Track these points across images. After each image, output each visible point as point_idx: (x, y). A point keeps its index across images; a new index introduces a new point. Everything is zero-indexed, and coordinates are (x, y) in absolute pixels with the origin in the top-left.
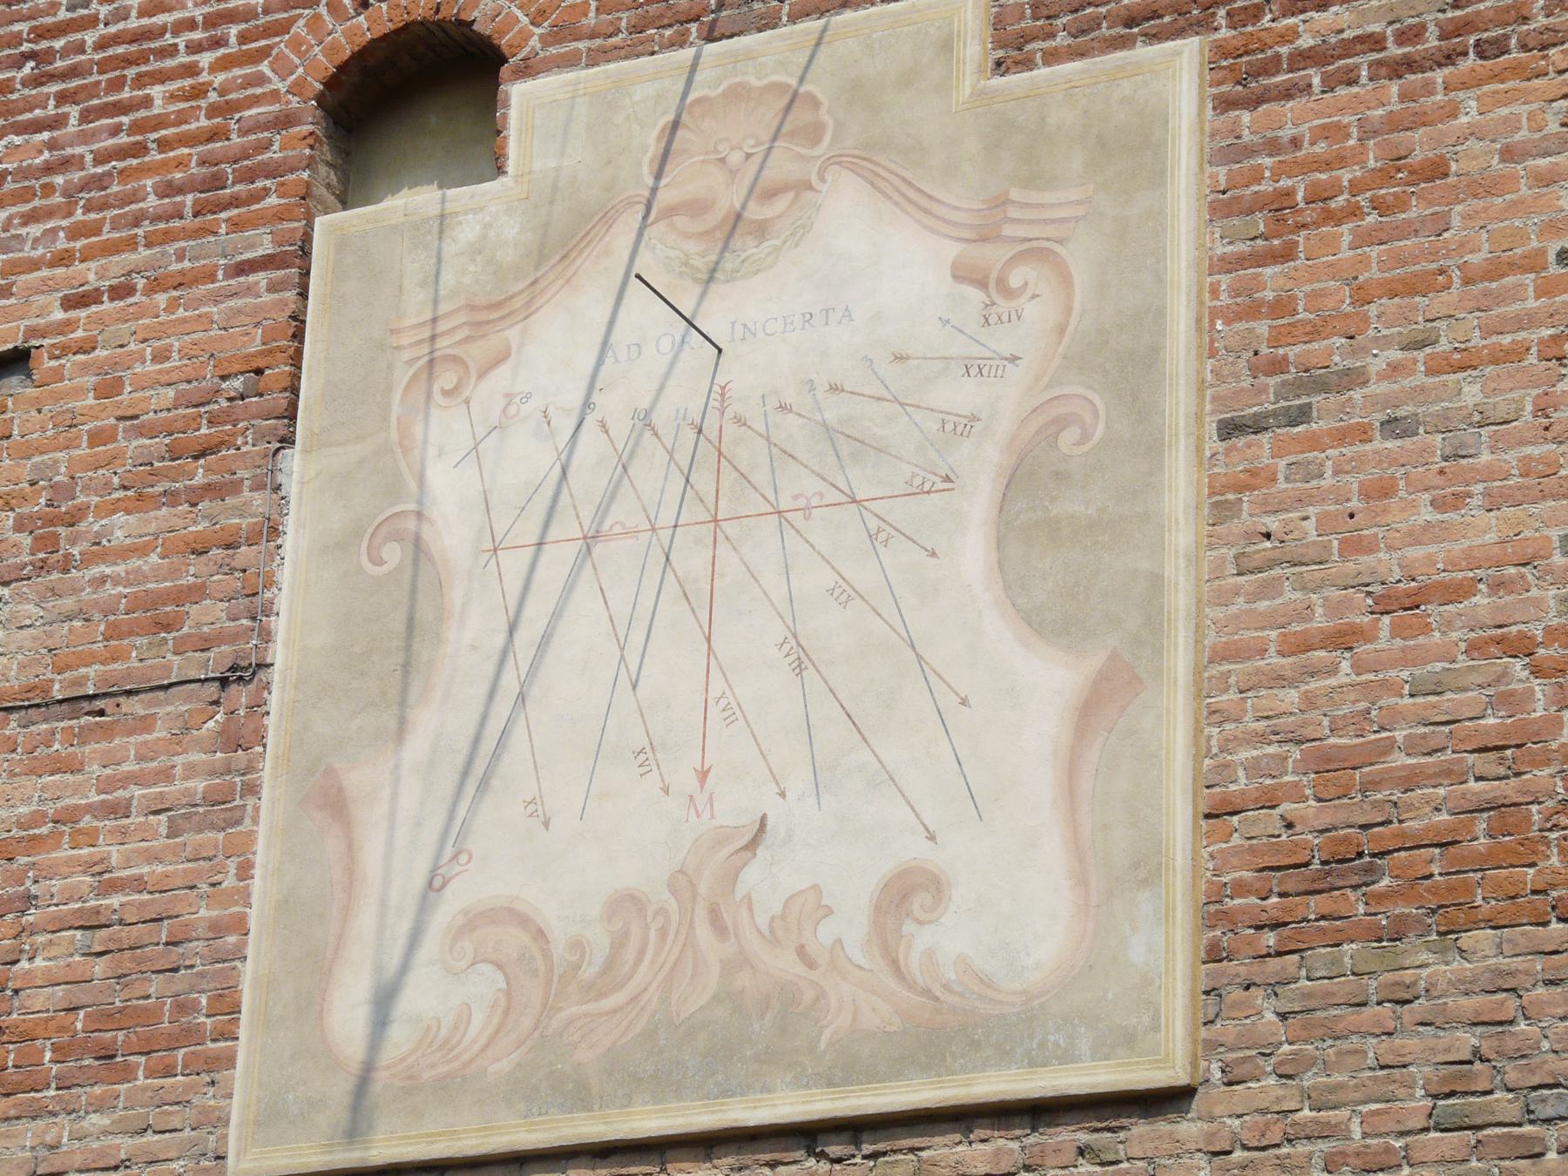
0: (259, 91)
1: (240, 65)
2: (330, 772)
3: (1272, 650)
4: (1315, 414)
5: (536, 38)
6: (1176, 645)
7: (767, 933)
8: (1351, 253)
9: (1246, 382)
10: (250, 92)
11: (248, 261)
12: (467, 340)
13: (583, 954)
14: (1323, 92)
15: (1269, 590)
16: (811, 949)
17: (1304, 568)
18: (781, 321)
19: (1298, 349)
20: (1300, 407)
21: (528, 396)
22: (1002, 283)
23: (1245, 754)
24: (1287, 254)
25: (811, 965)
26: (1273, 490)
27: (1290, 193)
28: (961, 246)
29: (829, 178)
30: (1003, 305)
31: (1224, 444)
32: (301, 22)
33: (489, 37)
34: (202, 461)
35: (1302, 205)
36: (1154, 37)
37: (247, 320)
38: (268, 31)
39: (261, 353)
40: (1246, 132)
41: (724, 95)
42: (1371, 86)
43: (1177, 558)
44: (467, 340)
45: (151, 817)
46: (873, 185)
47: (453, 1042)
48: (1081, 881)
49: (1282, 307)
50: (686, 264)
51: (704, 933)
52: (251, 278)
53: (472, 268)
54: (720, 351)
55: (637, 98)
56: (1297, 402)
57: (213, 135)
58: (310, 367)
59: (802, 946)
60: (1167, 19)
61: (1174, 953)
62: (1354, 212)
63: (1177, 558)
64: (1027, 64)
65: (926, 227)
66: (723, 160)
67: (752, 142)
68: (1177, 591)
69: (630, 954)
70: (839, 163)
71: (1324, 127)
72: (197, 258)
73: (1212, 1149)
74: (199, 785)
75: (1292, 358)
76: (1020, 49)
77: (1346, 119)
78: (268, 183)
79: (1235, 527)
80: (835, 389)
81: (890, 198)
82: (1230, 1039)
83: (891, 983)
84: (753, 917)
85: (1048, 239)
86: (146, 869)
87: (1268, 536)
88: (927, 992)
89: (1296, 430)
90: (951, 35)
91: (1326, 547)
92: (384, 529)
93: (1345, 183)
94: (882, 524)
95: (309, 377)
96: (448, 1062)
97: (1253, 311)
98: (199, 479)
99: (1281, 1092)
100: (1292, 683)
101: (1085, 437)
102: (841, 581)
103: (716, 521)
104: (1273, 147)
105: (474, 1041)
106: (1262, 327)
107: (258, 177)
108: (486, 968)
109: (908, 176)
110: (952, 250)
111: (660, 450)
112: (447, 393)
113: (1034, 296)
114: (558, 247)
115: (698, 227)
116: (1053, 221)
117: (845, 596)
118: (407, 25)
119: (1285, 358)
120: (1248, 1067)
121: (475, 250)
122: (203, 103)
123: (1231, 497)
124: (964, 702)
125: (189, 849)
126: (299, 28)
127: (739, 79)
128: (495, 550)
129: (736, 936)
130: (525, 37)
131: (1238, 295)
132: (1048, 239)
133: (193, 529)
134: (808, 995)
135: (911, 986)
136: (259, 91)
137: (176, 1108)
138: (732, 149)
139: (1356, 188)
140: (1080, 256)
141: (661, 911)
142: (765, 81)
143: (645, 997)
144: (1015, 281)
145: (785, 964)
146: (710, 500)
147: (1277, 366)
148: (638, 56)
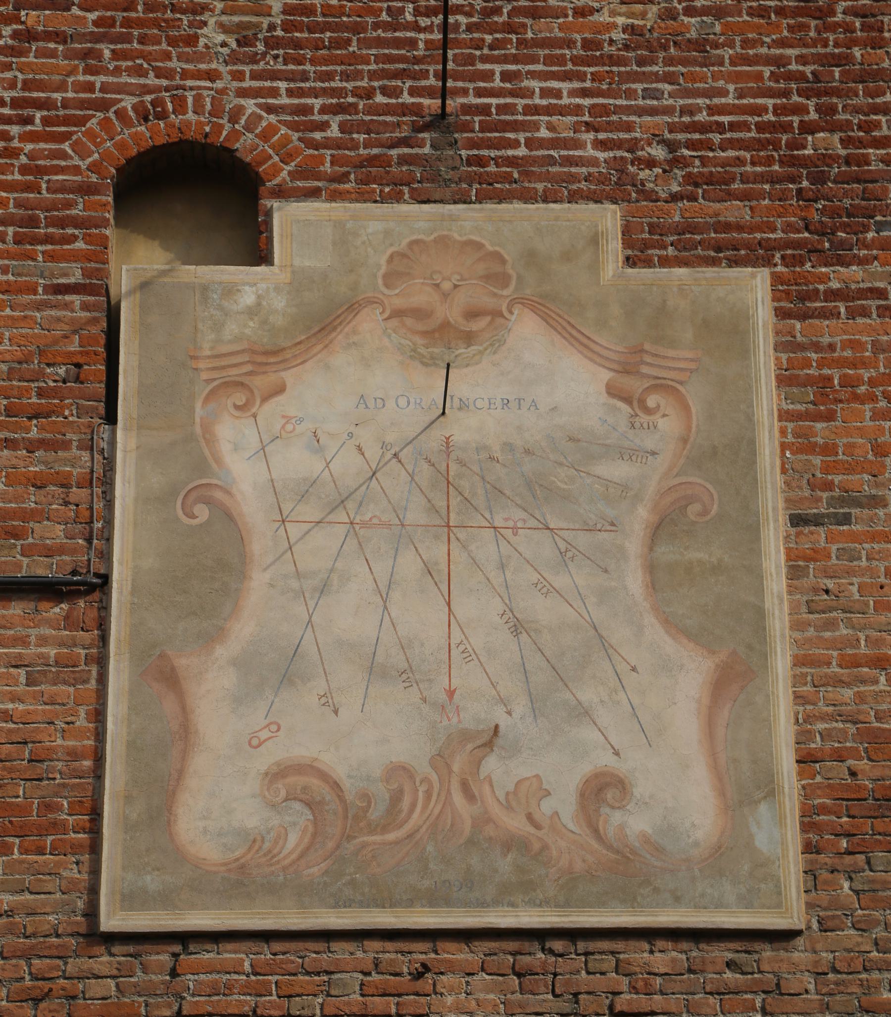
0: (63, 163)
1: (46, 141)
2: (162, 656)
3: (834, 663)
4: (853, 520)
5: (285, 172)
6: (776, 653)
7: (504, 802)
8: (872, 423)
9: (807, 493)
10: (55, 162)
11: (64, 285)
12: (250, 373)
13: (369, 802)
14: (848, 319)
15: (831, 625)
16: (537, 816)
17: (852, 615)
18: (487, 401)
19: (840, 477)
20: (844, 514)
21: (301, 420)
22: (642, 403)
23: (821, 726)
24: (830, 417)
25: (538, 827)
26: (829, 563)
27: (830, 379)
28: (611, 374)
29: (516, 312)
30: (644, 418)
31: (794, 529)
32: (94, 121)
33: (249, 164)
34: (35, 422)
35: (838, 388)
36: (734, 262)
37: (66, 327)
38: (67, 121)
39: (81, 352)
40: (798, 335)
41: (435, 241)
42: (878, 321)
43: (772, 598)
44: (250, 373)
45: (12, 670)
46: (547, 323)
47: (275, 851)
48: (721, 793)
49: (828, 449)
50: (414, 350)
51: (458, 798)
52: (68, 298)
53: (251, 324)
54: (443, 413)
55: (370, 230)
56: (842, 511)
57: (29, 187)
58: (125, 371)
59: (530, 814)
60: (743, 252)
61: (787, 846)
62: (873, 398)
63: (772, 598)
64: (648, 263)
65: (586, 357)
66: (437, 285)
67: (459, 278)
68: (774, 618)
69: (406, 804)
70: (522, 303)
71: (850, 341)
72: (19, 275)
73: (816, 971)
74: (52, 652)
75: (836, 483)
76: (642, 252)
77: (864, 339)
78: (76, 232)
79: (807, 582)
80: (527, 452)
81: (560, 333)
82: (825, 904)
83: (595, 844)
84: (493, 791)
85: (672, 380)
86: (10, 706)
87: (827, 592)
88: (618, 852)
89: (841, 528)
90: (596, 234)
91: (867, 604)
92: (194, 495)
93: (866, 379)
94: (569, 546)
95: (125, 378)
96: (271, 865)
97: (811, 449)
98: (34, 433)
99: (860, 940)
100: (848, 685)
101: (705, 512)
102: (542, 580)
103: (449, 526)
104: (817, 347)
105: (290, 853)
106: (817, 460)
107: (67, 226)
108: (297, 806)
109: (572, 321)
110: (606, 375)
111: (403, 472)
112: (237, 407)
113: (664, 416)
114: (323, 323)
115: (420, 327)
116: (675, 369)
117: (545, 590)
118: (181, 141)
119: (832, 482)
120: (837, 922)
121: (252, 312)
122: (16, 163)
123: (801, 563)
124: (634, 669)
125: (46, 696)
126: (92, 123)
127: (445, 233)
128: (283, 521)
129: (482, 801)
130: (277, 171)
131: (799, 437)
132: (672, 380)
133: (32, 469)
134: (536, 846)
135: (610, 848)
136: (63, 163)
137: (48, 877)
138: (443, 279)
139: (872, 382)
140: (696, 394)
141: (425, 780)
142: (464, 238)
143: (418, 836)
144: (651, 402)
145: (516, 824)
146: (444, 512)
147: (828, 486)
148: (365, 201)
